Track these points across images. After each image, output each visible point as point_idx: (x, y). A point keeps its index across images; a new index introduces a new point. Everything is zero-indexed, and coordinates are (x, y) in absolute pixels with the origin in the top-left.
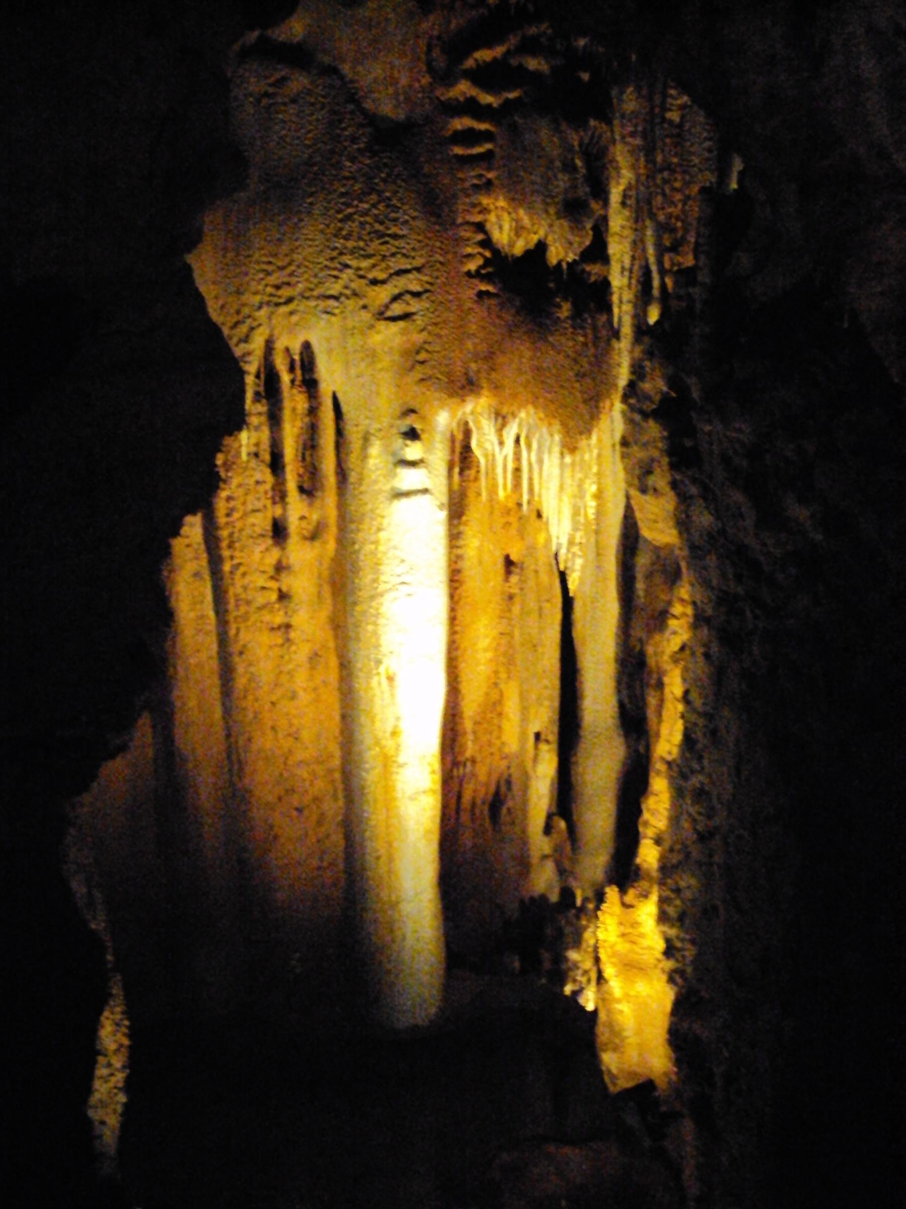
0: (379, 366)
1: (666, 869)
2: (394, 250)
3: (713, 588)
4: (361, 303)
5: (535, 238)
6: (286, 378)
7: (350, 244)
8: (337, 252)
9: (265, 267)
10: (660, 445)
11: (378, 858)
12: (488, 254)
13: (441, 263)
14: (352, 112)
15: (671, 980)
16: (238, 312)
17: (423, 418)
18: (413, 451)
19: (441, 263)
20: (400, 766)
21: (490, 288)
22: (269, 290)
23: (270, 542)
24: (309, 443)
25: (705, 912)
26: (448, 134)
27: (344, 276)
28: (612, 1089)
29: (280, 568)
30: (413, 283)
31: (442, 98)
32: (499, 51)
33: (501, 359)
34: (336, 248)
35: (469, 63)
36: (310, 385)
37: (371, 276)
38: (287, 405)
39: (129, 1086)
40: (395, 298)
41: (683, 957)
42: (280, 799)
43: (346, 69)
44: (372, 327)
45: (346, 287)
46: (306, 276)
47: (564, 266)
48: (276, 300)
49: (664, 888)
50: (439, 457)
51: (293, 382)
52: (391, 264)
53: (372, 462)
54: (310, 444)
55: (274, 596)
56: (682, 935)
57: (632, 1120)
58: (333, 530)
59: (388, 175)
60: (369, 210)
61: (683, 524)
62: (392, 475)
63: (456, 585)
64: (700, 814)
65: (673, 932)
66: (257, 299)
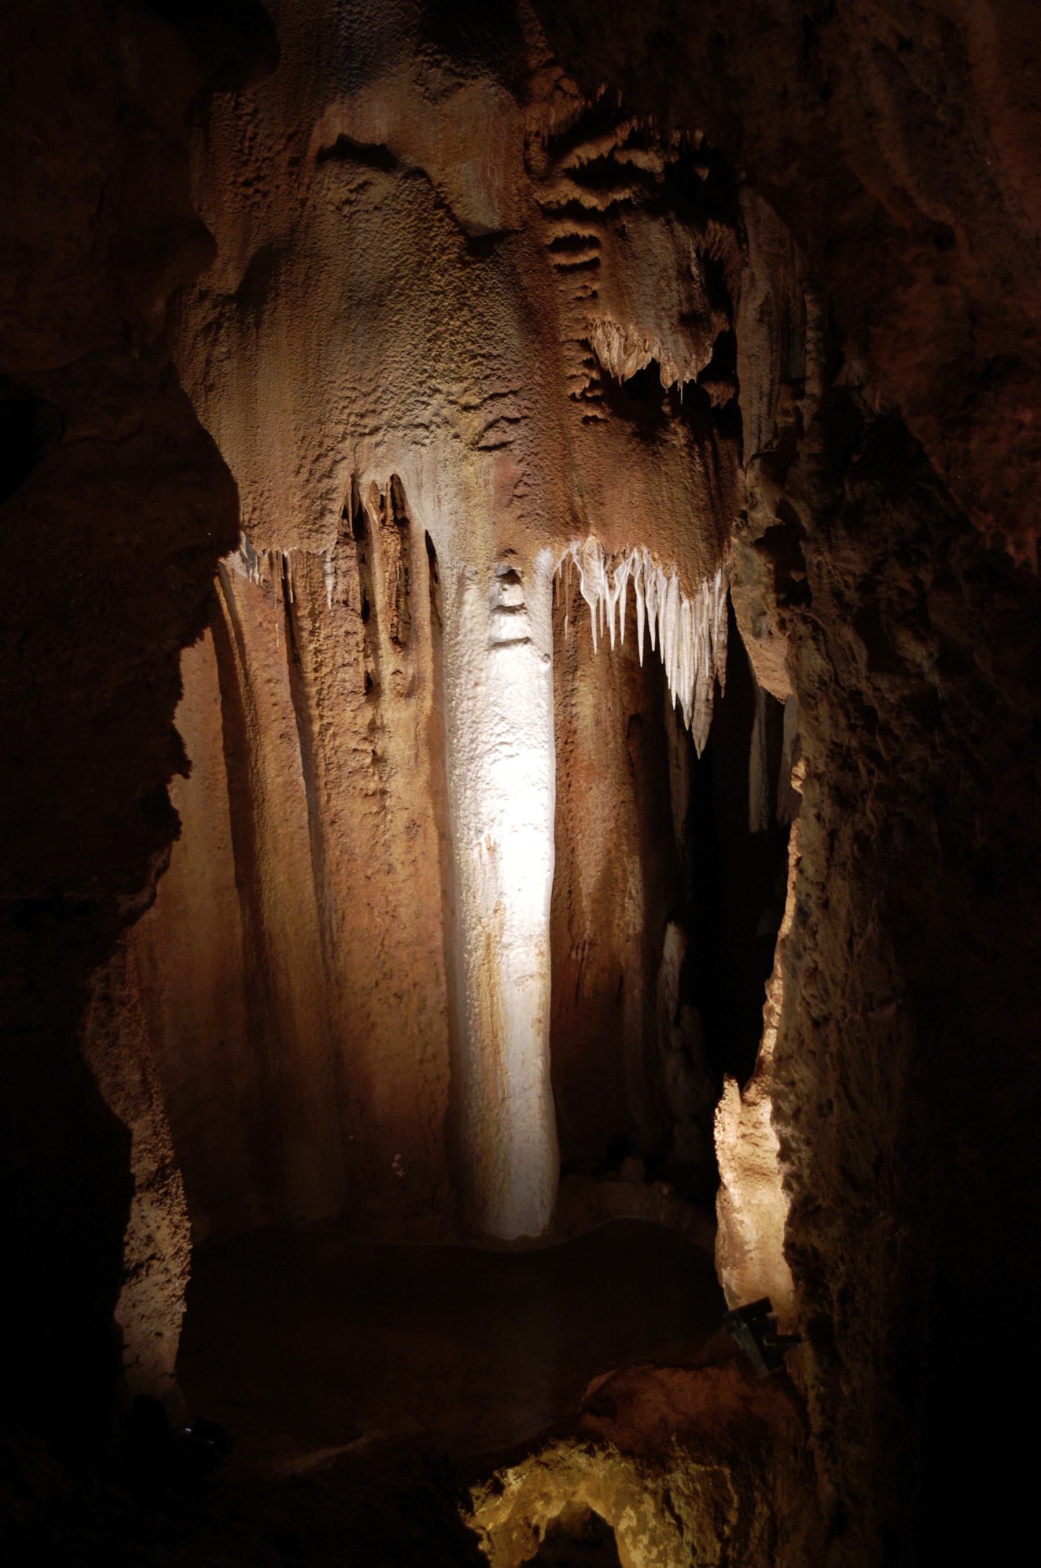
0: (473, 502)
1: (782, 1058)
2: (489, 371)
3: (823, 740)
4: (453, 431)
5: (649, 357)
6: (374, 517)
7: (440, 366)
8: (426, 375)
9: (348, 393)
10: (765, 580)
11: (483, 1049)
12: (595, 375)
13: (540, 385)
14: (441, 220)
15: (787, 1186)
16: (321, 445)
17: (524, 560)
18: (512, 596)
19: (540, 385)
20: (506, 947)
21: (598, 413)
22: (353, 419)
23: (363, 699)
24: (403, 589)
25: (820, 1107)
26: (548, 241)
27: (433, 402)
28: (731, 1307)
29: (374, 728)
30: (508, 408)
31: (542, 202)
32: (605, 147)
33: (609, 493)
34: (425, 371)
35: (572, 161)
36: (402, 523)
37: (463, 401)
38: (376, 545)
39: (190, 1294)
40: (490, 426)
41: (800, 1159)
42: (377, 984)
43: (433, 171)
44: (465, 457)
45: (436, 415)
46: (393, 403)
47: (680, 386)
48: (360, 430)
49: (778, 1081)
50: (541, 602)
51: (383, 521)
52: (485, 388)
53: (467, 608)
54: (403, 592)
55: (368, 760)
56: (797, 1134)
57: (745, 1342)
58: (429, 686)
59: (482, 289)
60: (460, 327)
61: (794, 669)
62: (489, 623)
63: (569, 747)
64: (814, 997)
65: (788, 1131)
66: (341, 428)
